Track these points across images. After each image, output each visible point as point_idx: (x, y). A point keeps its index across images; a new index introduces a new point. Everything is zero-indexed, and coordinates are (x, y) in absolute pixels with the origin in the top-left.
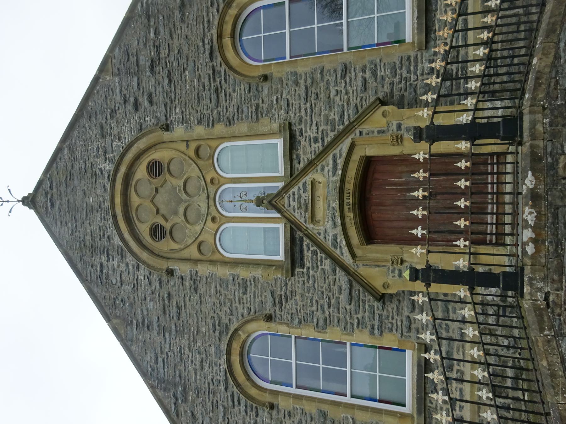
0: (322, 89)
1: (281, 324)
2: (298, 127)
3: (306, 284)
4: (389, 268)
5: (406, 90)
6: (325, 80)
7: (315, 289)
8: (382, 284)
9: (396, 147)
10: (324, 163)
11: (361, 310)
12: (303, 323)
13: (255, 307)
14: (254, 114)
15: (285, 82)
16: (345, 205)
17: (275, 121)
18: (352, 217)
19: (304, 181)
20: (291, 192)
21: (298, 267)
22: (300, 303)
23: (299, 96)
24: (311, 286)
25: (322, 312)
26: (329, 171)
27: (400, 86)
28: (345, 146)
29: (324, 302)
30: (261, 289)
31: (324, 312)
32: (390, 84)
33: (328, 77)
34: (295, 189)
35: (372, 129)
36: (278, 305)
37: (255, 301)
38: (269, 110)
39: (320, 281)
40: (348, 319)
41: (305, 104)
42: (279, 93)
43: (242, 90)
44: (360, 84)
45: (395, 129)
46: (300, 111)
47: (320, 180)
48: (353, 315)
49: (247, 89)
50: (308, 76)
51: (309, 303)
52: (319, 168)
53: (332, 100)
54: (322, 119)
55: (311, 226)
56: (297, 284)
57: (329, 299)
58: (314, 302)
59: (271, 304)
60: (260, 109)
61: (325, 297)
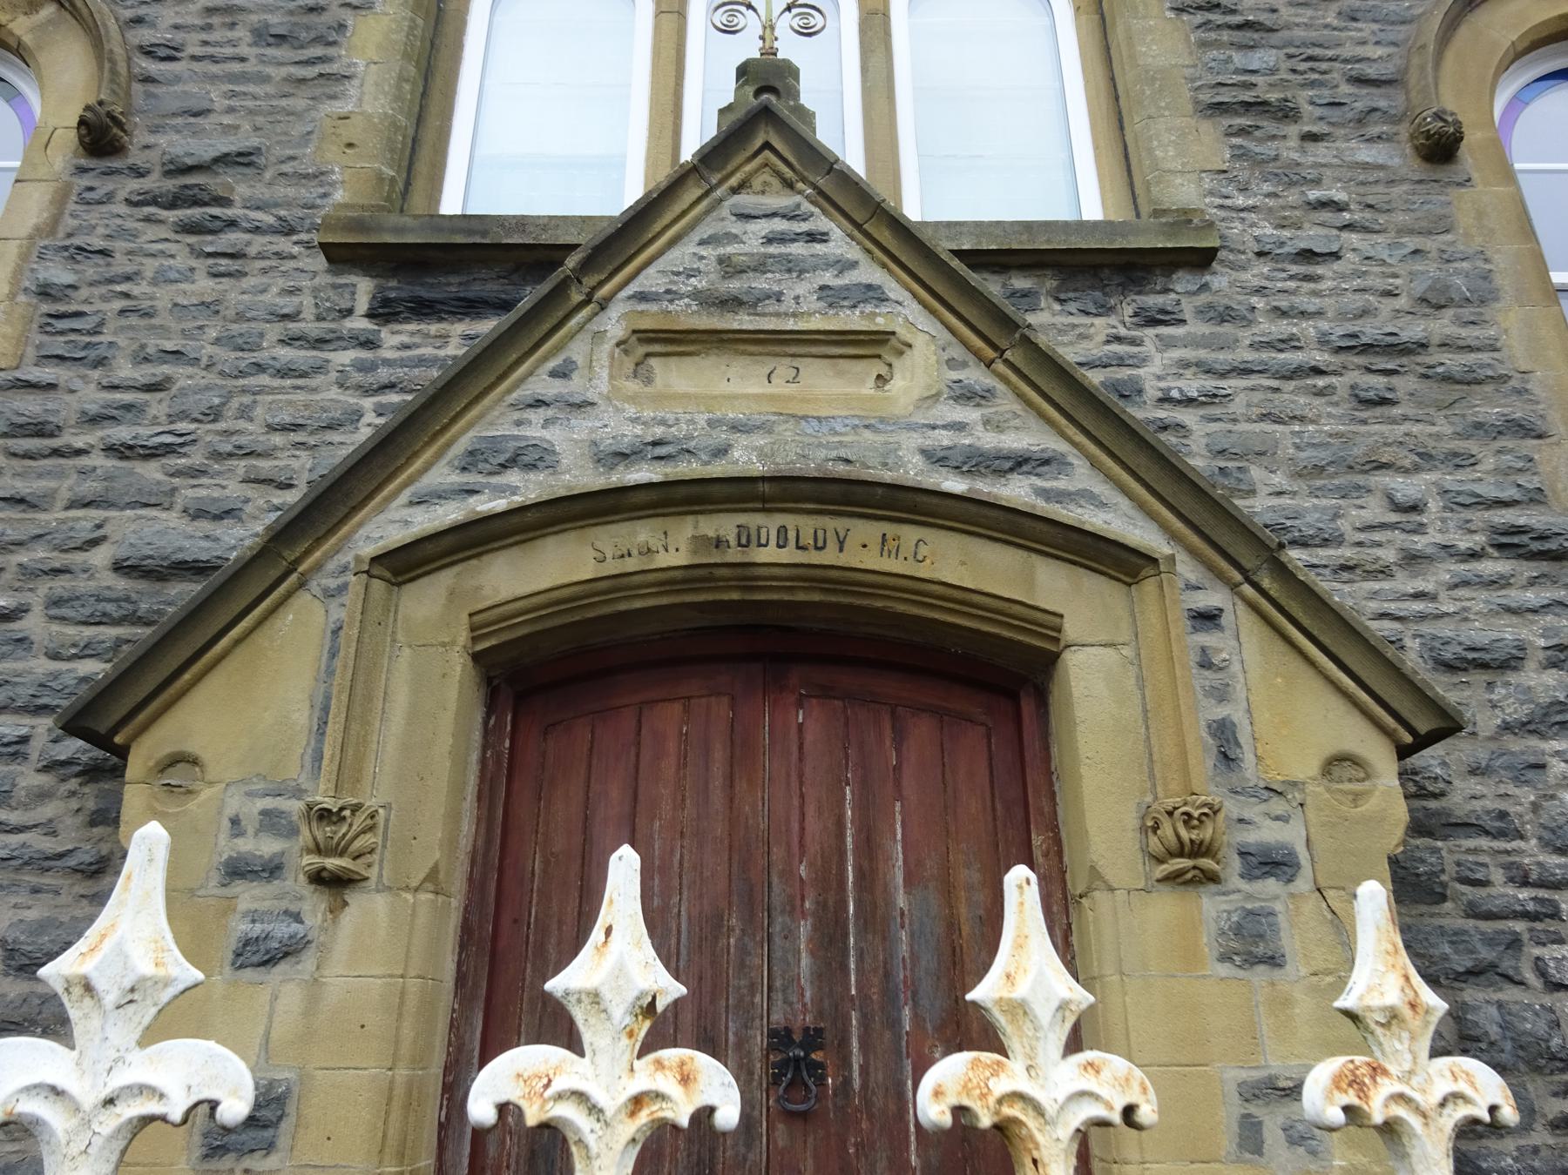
0: (1416, 429)
1: (60, 200)
2: (1187, 308)
3: (274, 331)
4: (298, 793)
5: (1473, 911)
6: (1472, 446)
7: (243, 374)
8: (191, 747)
9: (1130, 841)
10: (1006, 403)
11: (71, 631)
12: (46, 308)
13: (178, 79)
14: (1247, 96)
15: (1429, 244)
16: (742, 519)
17: (1211, 193)
18: (665, 560)
19: (893, 289)
20: (822, 223)
21: (380, 289)
22: (163, 297)
23: (1364, 313)
24: (260, 357)
25: (93, 409)
26: (959, 427)
27: (1497, 876)
28: (1119, 518)
29: (155, 421)
30: (274, 111)
31: (95, 420)
32: (1503, 815)
33: (1489, 463)
34: (840, 244)
35: (1240, 691)
36: (171, 185)
37: (213, 78)
38: (1271, 167)
39: (287, 402)
40: (23, 557)
41: (1323, 341)
42: (1368, 214)
43: (1360, 51)
44: (1478, 633)
45: (1251, 837)
46: (1282, 313)
47: (897, 384)
48: (45, 587)
49: (1371, 71)
50: (1485, 357)
51: (153, 344)
52: (976, 376)
53: (1360, 479)
54: (1243, 427)
55: (614, 323)
56: (281, 283)
57: (169, 450)
58: (166, 369)
59: (178, 150)
60: (1269, 126)
61: (183, 426)
